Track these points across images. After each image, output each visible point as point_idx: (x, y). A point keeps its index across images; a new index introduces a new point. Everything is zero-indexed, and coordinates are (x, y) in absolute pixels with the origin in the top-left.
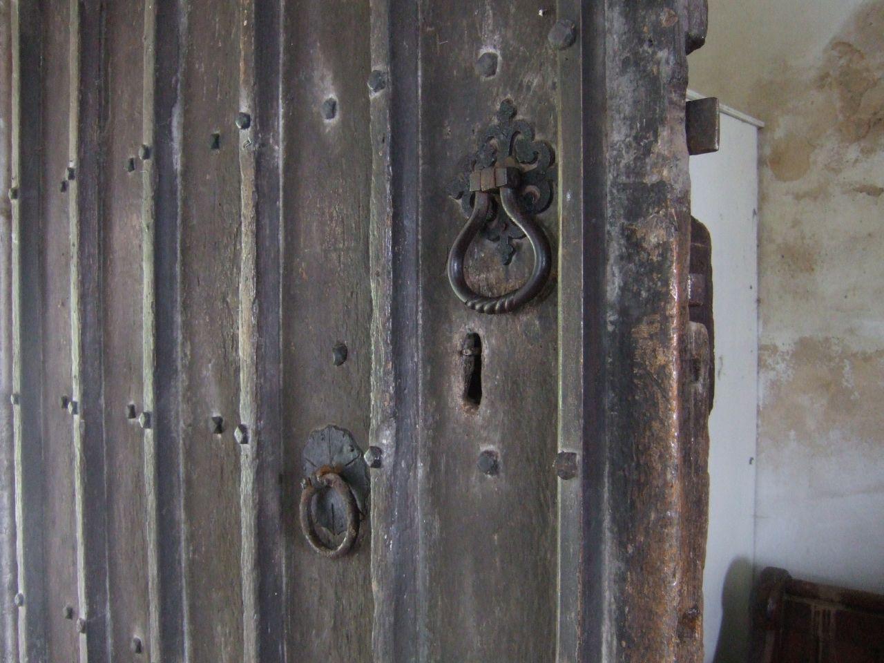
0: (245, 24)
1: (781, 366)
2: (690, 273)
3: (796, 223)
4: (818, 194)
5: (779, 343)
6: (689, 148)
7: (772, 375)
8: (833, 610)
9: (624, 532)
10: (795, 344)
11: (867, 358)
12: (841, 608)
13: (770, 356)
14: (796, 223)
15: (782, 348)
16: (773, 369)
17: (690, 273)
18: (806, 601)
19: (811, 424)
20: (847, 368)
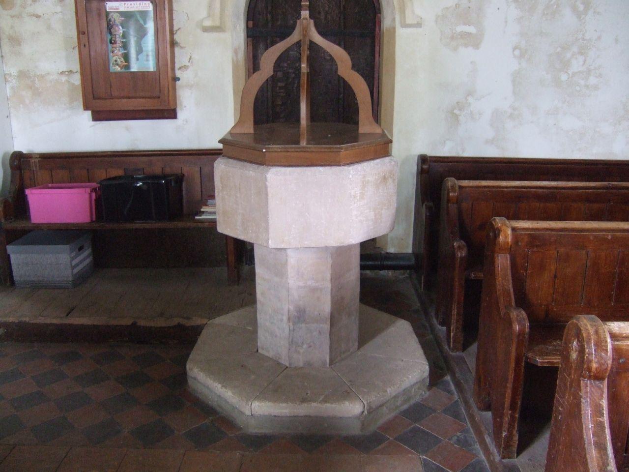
0: (621, 361)
1: (14, 81)
2: (482, 281)
3: (12, 27)
4: (19, 16)
5: (12, 73)
6: (557, 371)
7: (11, 84)
8: (37, 160)
9: (588, 197)
10: (18, 72)
11: (43, 77)
12: (40, 159)
13: (9, 77)
14: (12, 27)
15: (13, 74)
16: (11, 82)
17: (481, 281)
18: (29, 159)
19: (27, 101)
20: (37, 81)
